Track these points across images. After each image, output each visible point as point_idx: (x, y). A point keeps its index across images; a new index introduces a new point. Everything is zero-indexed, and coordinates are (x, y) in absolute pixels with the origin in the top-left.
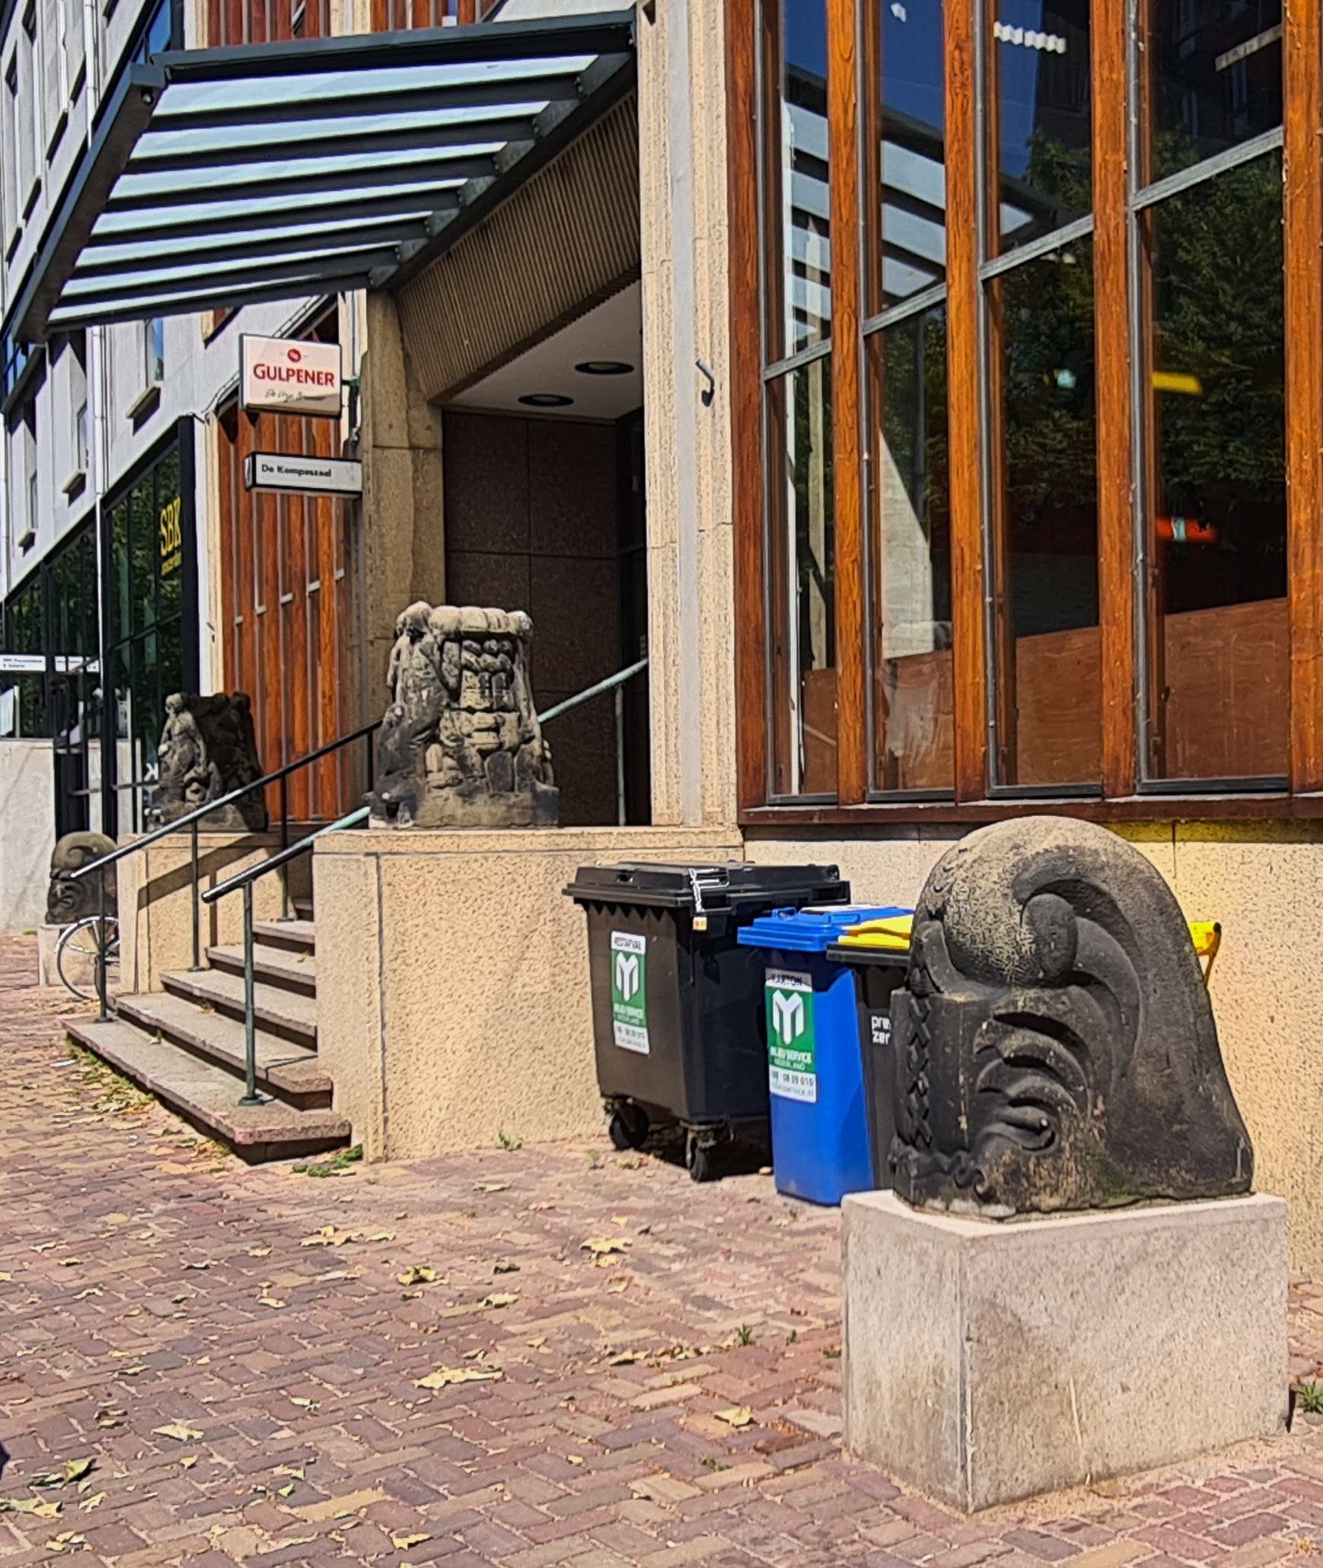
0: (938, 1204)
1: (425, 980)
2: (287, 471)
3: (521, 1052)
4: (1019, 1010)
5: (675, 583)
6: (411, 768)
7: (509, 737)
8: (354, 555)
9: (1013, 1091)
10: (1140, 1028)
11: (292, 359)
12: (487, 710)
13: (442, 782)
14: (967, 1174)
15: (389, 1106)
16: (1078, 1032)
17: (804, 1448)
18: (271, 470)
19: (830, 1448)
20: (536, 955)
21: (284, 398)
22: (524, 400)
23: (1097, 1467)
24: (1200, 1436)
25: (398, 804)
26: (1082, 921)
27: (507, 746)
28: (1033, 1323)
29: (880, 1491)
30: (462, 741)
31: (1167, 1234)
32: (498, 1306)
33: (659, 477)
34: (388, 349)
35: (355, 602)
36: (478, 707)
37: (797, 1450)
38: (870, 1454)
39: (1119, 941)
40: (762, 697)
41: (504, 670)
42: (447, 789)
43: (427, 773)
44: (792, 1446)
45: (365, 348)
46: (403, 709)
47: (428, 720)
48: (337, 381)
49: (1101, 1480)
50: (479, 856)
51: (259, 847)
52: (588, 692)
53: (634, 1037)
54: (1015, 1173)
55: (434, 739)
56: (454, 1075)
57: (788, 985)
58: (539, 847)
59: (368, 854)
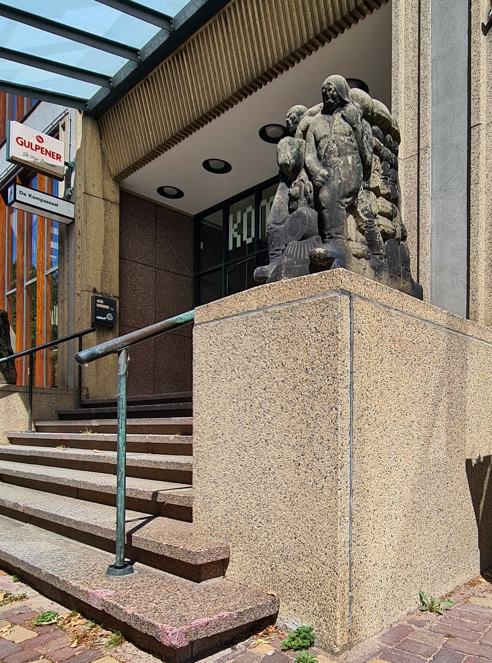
8: (66, 253)
13: (360, 251)
18: (25, 195)
22: (161, 191)
35: (66, 276)
51: (15, 392)
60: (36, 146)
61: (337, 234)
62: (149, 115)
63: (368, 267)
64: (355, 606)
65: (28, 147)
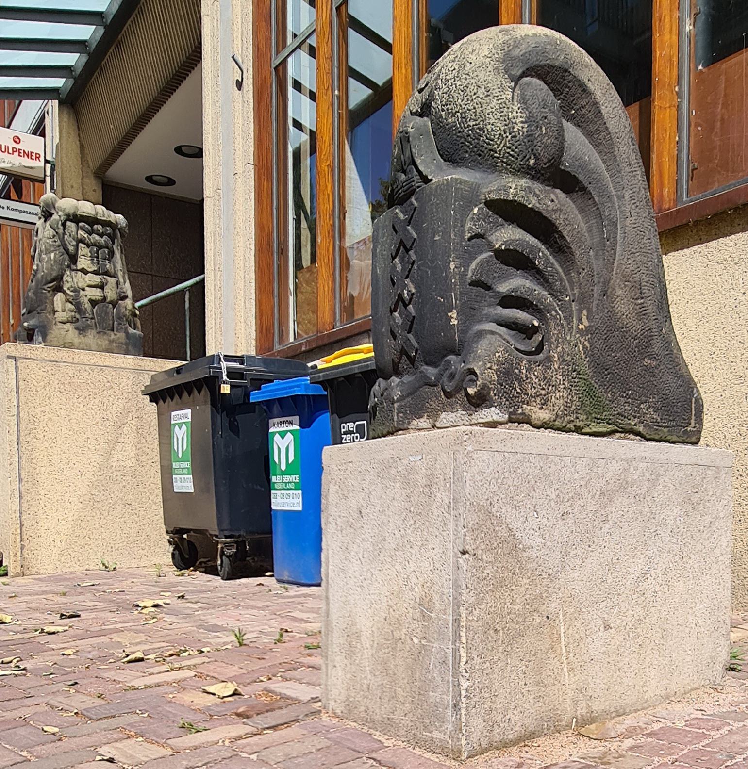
0: (424, 422)
1: (50, 450)
2: (12, 209)
3: (117, 506)
4: (511, 198)
5: (220, 216)
6: (43, 307)
7: (111, 293)
9: (504, 288)
10: (619, 249)
11: (15, 142)
12: (95, 273)
13: (65, 319)
14: (457, 377)
15: (25, 537)
16: (565, 233)
17: (284, 711)
19: (311, 711)
20: (126, 440)
21: (10, 165)
22: (149, 179)
23: (582, 710)
24: (666, 681)
25: (33, 330)
26: (568, 126)
27: (108, 300)
28: (528, 542)
29: (362, 744)
30: (79, 292)
31: (643, 465)
32: (49, 633)
33: (211, 151)
34: (71, 140)
36: (89, 270)
37: (278, 713)
38: (350, 711)
39: (600, 153)
40: (271, 282)
41: (107, 248)
42: (68, 324)
43: (55, 312)
44: (272, 710)
45: (57, 141)
46: (38, 265)
47: (54, 274)
48: (42, 159)
49: (583, 725)
50: (87, 368)
52: (168, 291)
53: (184, 484)
54: (507, 374)
55: (59, 289)
56: (70, 519)
57: (284, 428)
58: (128, 366)
59: (9, 357)
60: (13, 148)
61: (41, 310)
62: (114, 105)
63: (71, 329)
64: (25, 551)
65: (5, 152)
